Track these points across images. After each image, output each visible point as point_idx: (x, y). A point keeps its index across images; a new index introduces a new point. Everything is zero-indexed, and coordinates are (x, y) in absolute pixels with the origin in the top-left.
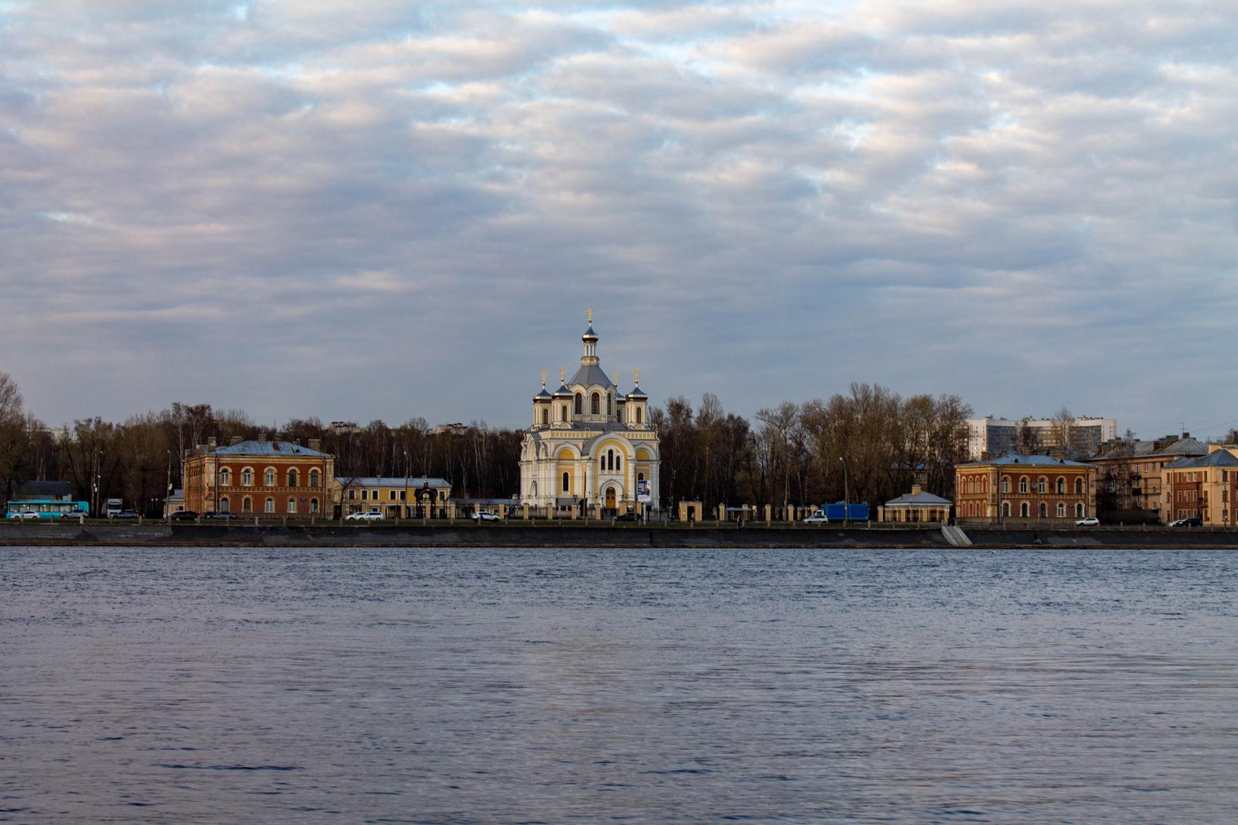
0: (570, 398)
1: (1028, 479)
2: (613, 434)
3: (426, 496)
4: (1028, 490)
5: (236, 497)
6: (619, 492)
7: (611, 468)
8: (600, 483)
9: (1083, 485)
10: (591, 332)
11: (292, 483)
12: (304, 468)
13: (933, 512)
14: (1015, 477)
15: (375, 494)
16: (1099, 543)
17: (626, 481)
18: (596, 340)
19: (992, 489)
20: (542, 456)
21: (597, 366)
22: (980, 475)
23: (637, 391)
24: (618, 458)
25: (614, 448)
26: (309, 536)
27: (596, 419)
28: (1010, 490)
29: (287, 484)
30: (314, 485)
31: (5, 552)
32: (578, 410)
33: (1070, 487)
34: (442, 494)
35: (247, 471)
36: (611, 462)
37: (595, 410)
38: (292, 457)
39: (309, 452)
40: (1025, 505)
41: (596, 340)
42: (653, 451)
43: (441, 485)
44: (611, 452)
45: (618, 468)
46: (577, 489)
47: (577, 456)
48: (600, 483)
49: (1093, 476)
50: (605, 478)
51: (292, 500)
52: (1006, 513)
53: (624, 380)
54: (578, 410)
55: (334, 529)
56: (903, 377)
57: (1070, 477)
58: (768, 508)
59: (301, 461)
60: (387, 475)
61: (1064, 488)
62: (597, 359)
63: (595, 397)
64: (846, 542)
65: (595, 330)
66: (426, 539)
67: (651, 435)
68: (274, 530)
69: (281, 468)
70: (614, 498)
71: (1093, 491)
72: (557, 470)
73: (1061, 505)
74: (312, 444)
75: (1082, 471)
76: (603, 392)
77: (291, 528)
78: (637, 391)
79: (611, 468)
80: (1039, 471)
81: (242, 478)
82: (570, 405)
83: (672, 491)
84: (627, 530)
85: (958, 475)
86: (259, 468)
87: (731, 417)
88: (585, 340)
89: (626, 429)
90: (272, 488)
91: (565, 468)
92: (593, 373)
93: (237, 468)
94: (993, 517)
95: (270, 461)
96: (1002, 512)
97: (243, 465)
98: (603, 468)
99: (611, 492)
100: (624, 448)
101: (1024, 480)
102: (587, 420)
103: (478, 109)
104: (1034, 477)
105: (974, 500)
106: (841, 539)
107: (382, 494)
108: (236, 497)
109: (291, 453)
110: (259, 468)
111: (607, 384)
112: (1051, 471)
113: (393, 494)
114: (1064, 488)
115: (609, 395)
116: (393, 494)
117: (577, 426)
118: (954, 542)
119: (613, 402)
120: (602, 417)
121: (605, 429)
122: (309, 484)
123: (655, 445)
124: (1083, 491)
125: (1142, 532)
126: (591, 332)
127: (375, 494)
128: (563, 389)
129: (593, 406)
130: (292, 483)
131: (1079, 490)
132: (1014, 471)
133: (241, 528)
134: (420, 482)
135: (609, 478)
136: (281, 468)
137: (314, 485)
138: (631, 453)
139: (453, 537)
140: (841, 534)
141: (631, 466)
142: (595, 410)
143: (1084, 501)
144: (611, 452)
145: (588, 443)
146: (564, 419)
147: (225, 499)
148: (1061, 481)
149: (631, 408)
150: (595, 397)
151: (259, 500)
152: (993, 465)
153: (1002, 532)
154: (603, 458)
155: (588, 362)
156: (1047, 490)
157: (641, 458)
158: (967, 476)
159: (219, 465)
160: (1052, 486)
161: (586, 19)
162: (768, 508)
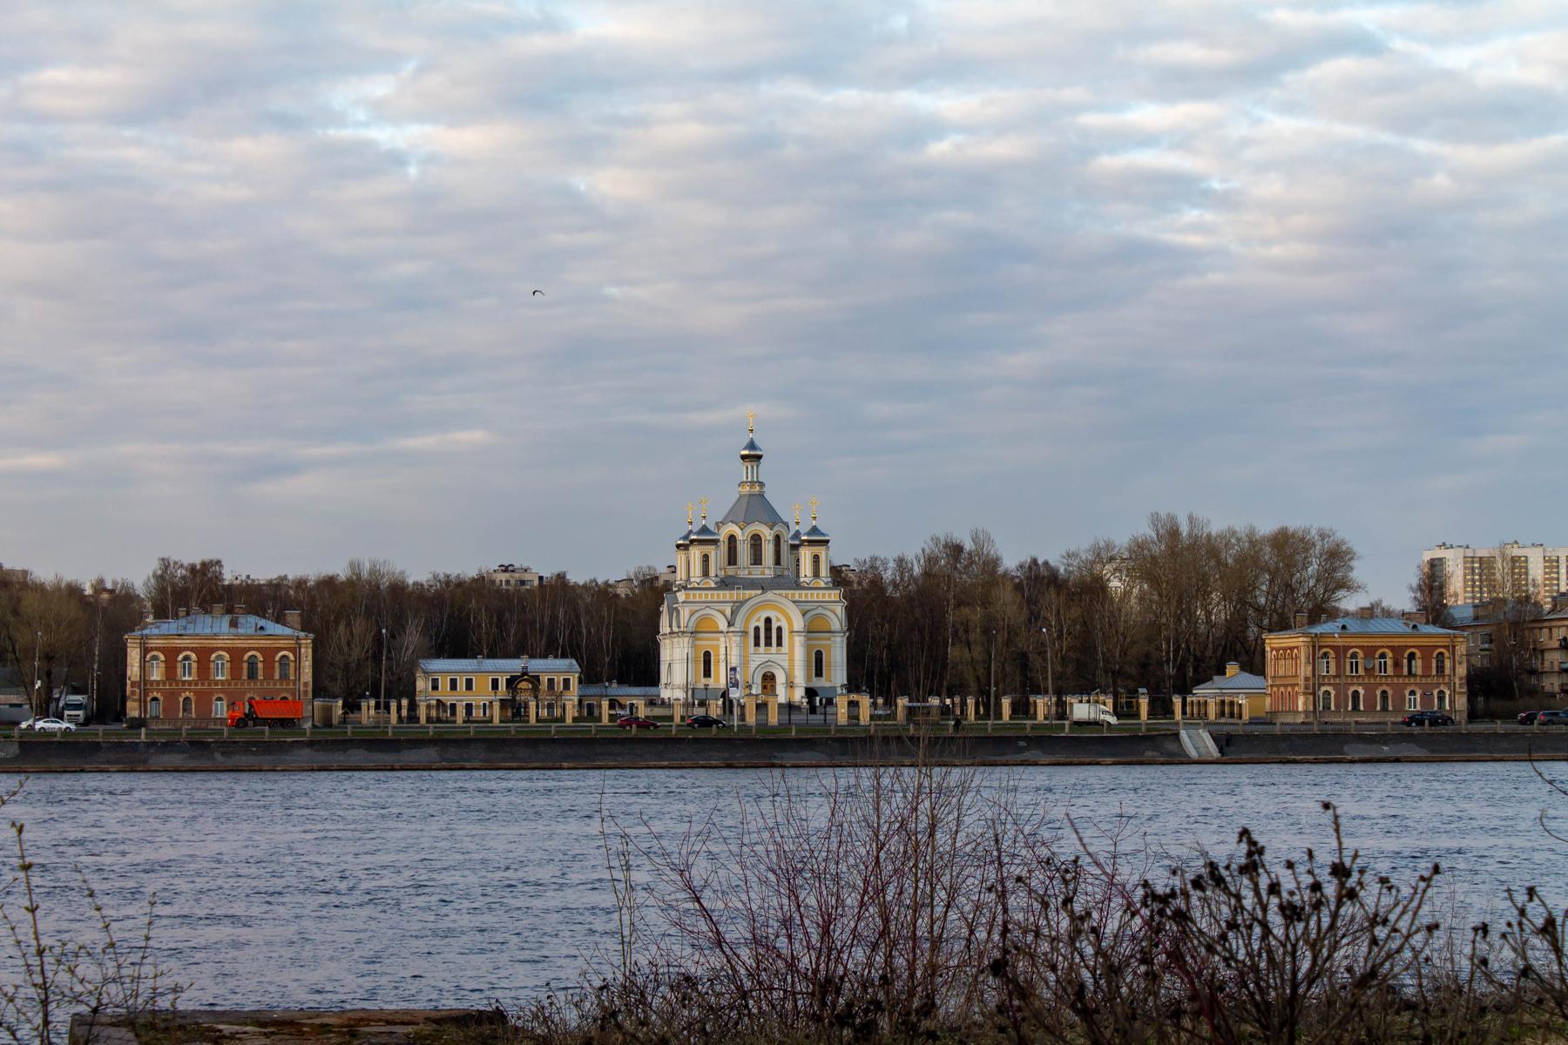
0: (715, 542)
1: (1361, 654)
2: (770, 595)
3: (523, 685)
4: (1361, 672)
5: (172, 696)
6: (781, 678)
7: (768, 644)
8: (753, 666)
9: (1448, 664)
10: (752, 446)
11: (252, 675)
12: (269, 653)
13: (1223, 702)
14: (1340, 651)
15: (469, 683)
16: (1423, 753)
17: (792, 660)
18: (760, 457)
19: (1305, 670)
20: (675, 629)
21: (761, 495)
22: (1292, 649)
23: (815, 530)
24: (779, 629)
25: (772, 614)
26: (218, 756)
27: (757, 573)
28: (1333, 671)
29: (245, 677)
30: (284, 677)
31: (4, 776)
32: (732, 559)
33: (1426, 667)
34: (551, 681)
35: (187, 658)
36: (769, 635)
37: (757, 559)
38: (250, 637)
39: (279, 629)
40: (1356, 693)
41: (760, 457)
42: (836, 616)
43: (558, 669)
44: (768, 621)
45: (779, 644)
46: (719, 679)
47: (723, 625)
48: (753, 666)
49: (1461, 649)
50: (760, 658)
51: (219, 699)
52: (1327, 707)
53: (797, 515)
54: (732, 559)
55: (256, 743)
56: (1235, 503)
57: (1426, 651)
58: (970, 701)
59: (196, 643)
60: (492, 655)
61: (1418, 666)
62: (762, 484)
63: (756, 540)
64: (1027, 755)
65: (757, 443)
66: (388, 758)
67: (834, 595)
68: (169, 747)
69: (236, 654)
70: (774, 687)
71: (1462, 670)
72: (694, 647)
73: (1413, 693)
74: (289, 618)
75: (1446, 642)
76: (767, 534)
77: (192, 743)
78: (815, 530)
79: (768, 644)
80: (1378, 642)
81: (179, 670)
82: (717, 556)
83: (867, 671)
84: (696, 740)
85: (1268, 649)
86: (204, 654)
87: (1046, 563)
88: (744, 457)
89: (797, 586)
90: (223, 683)
91: (705, 644)
92: (756, 505)
93: (171, 654)
94: (1306, 712)
95: (220, 643)
96: (1320, 706)
97: (179, 650)
98: (757, 644)
99: (769, 679)
100: (791, 619)
101: (1354, 656)
102: (743, 574)
103: (1182, 140)
104: (1369, 652)
105: (1285, 686)
106: (1021, 750)
107: (465, 686)
108: (172, 696)
109: (251, 631)
110: (204, 654)
111: (773, 519)
112: (1396, 642)
113: (495, 684)
114: (1418, 666)
115: (777, 539)
116: (495, 684)
117: (724, 584)
118: (1193, 754)
119: (784, 548)
120: (767, 570)
121: (763, 586)
122: (277, 676)
123: (840, 609)
124: (1447, 671)
125: (1496, 734)
126: (752, 446)
127: (469, 683)
128: (705, 530)
129: (757, 550)
130: (252, 675)
131: (1440, 669)
132: (1340, 642)
133: (120, 745)
134: (515, 665)
135: (766, 658)
136: (236, 654)
137: (284, 677)
138: (799, 624)
139: (431, 753)
140: (1022, 744)
141: (799, 640)
142: (757, 559)
143: (1448, 685)
144: (768, 621)
145: (737, 606)
146: (706, 573)
147: (155, 699)
148: (1412, 656)
149: (806, 554)
150: (756, 540)
151: (205, 699)
152: (1305, 635)
153: (1273, 737)
154: (757, 629)
155: (747, 489)
156: (1390, 671)
157: (813, 630)
158: (1278, 650)
159: (145, 651)
160: (1397, 665)
161: (1365, 18)
162: (970, 701)
